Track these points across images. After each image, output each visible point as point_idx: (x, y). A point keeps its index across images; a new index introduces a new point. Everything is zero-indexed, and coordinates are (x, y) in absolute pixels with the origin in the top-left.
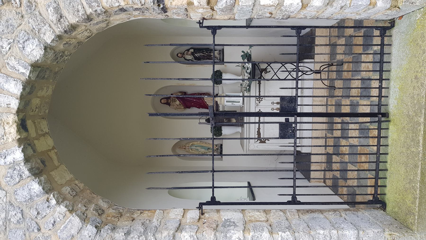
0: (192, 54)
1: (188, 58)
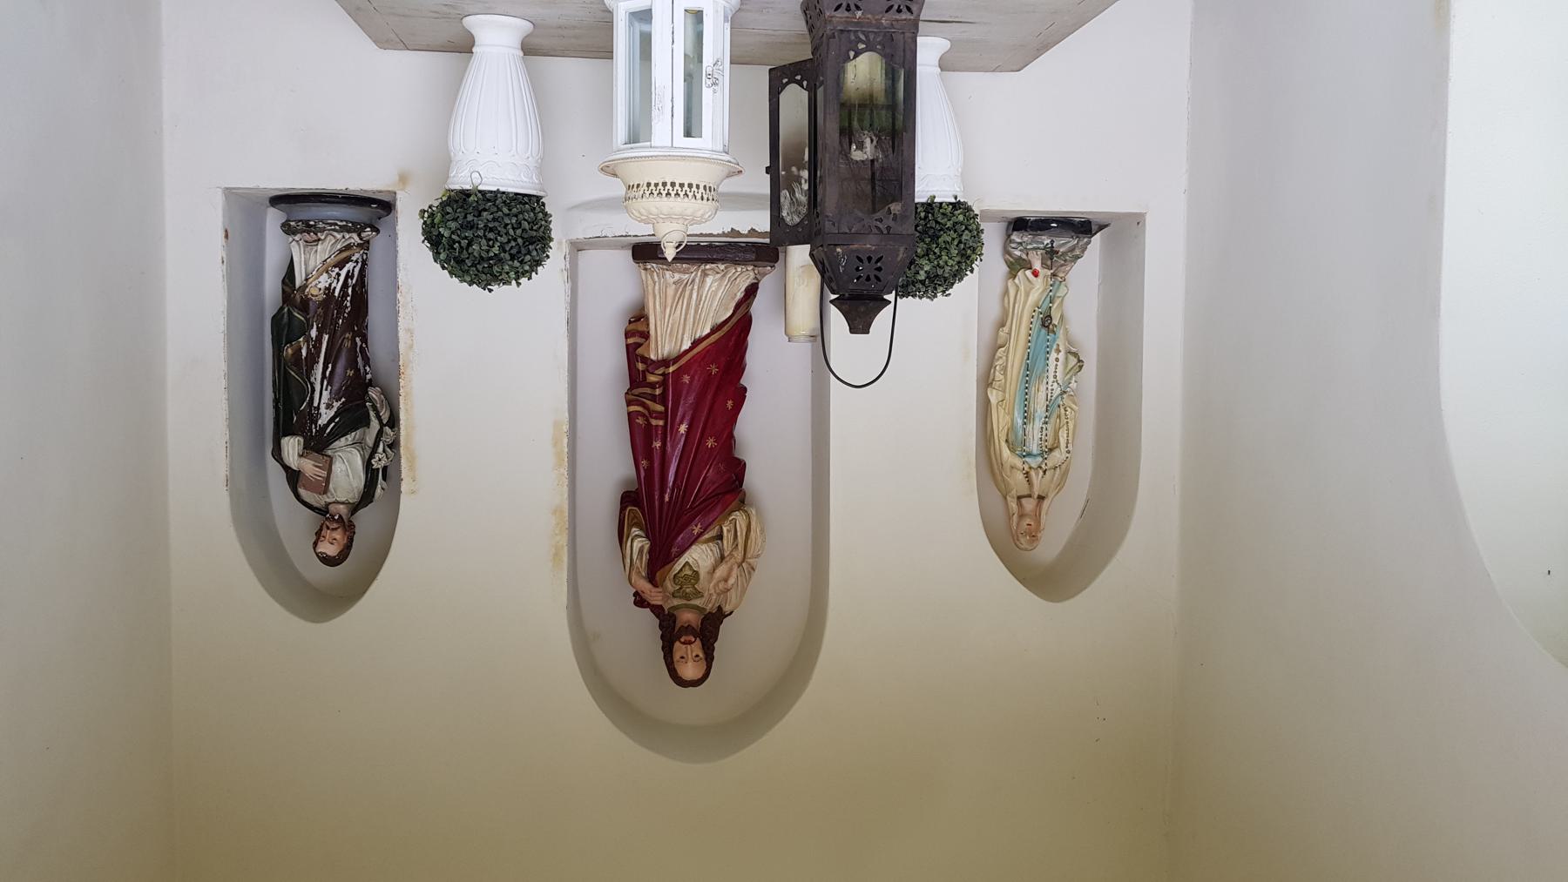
0: (318, 445)
1: (358, 481)
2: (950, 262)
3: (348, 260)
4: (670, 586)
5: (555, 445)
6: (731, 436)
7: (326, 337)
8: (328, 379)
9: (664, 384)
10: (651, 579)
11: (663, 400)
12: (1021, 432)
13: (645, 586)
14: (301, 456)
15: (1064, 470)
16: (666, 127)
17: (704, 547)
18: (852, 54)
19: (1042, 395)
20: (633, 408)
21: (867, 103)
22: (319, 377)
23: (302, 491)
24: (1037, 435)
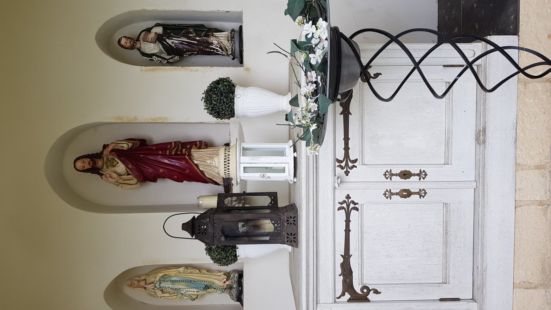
0: (159, 39)
1: (148, 51)
2: (215, 255)
3: (222, 50)
4: (110, 157)
5: (159, 118)
6: (164, 178)
7: (196, 42)
8: (182, 43)
9: (182, 154)
10: (113, 150)
11: (176, 154)
12: (168, 280)
13: (110, 148)
14: (156, 33)
15: (155, 296)
16: (246, 161)
17: (124, 169)
18: (273, 222)
19: (181, 287)
20: (173, 144)
21: (257, 227)
22: (183, 40)
23: (144, 33)
24: (167, 286)
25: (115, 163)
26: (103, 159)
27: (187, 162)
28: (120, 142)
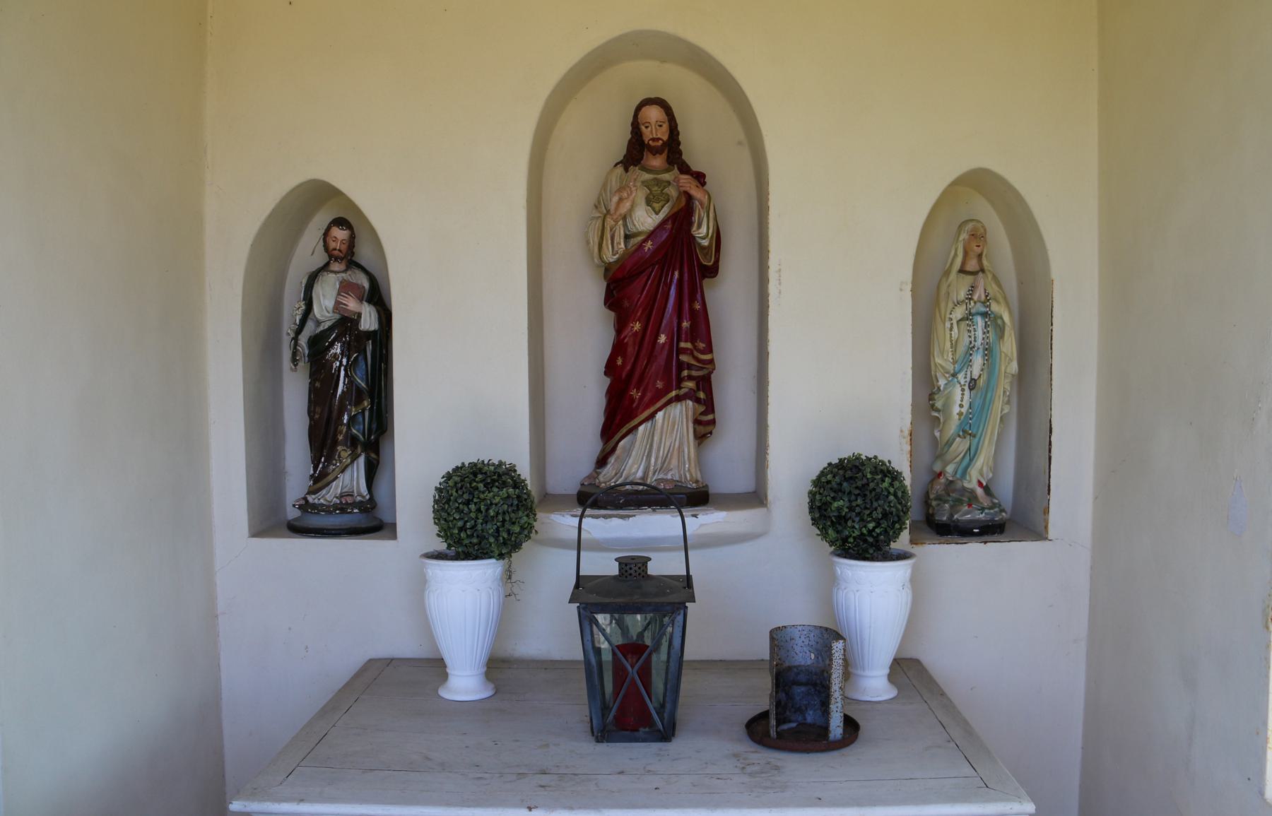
0: (346, 323)
4: (672, 192)
9: (680, 380)
10: (690, 198)
11: (681, 365)
13: (696, 193)
14: (359, 315)
17: (641, 228)
25: (657, 206)
26: (667, 171)
27: (659, 395)
28: (711, 215)
